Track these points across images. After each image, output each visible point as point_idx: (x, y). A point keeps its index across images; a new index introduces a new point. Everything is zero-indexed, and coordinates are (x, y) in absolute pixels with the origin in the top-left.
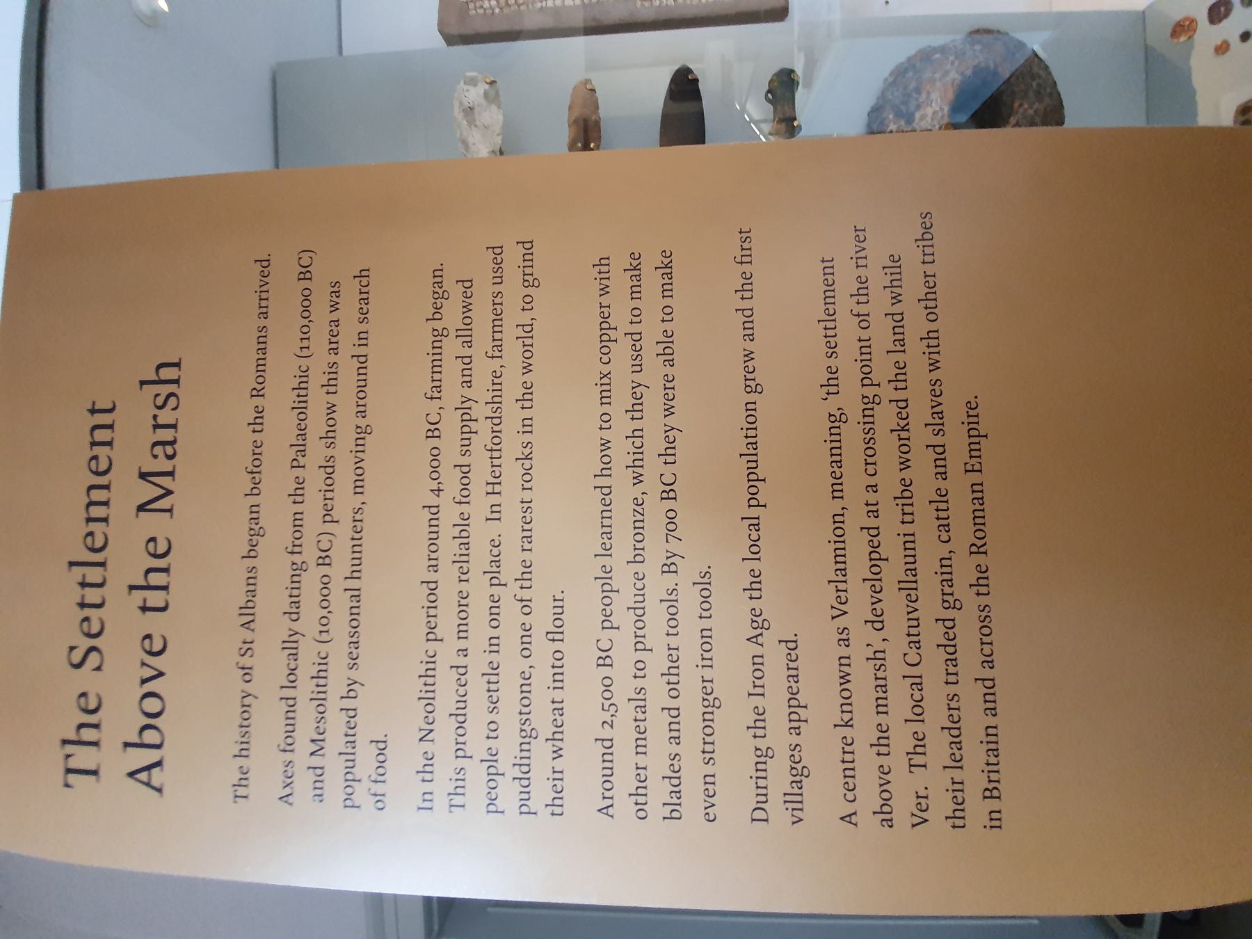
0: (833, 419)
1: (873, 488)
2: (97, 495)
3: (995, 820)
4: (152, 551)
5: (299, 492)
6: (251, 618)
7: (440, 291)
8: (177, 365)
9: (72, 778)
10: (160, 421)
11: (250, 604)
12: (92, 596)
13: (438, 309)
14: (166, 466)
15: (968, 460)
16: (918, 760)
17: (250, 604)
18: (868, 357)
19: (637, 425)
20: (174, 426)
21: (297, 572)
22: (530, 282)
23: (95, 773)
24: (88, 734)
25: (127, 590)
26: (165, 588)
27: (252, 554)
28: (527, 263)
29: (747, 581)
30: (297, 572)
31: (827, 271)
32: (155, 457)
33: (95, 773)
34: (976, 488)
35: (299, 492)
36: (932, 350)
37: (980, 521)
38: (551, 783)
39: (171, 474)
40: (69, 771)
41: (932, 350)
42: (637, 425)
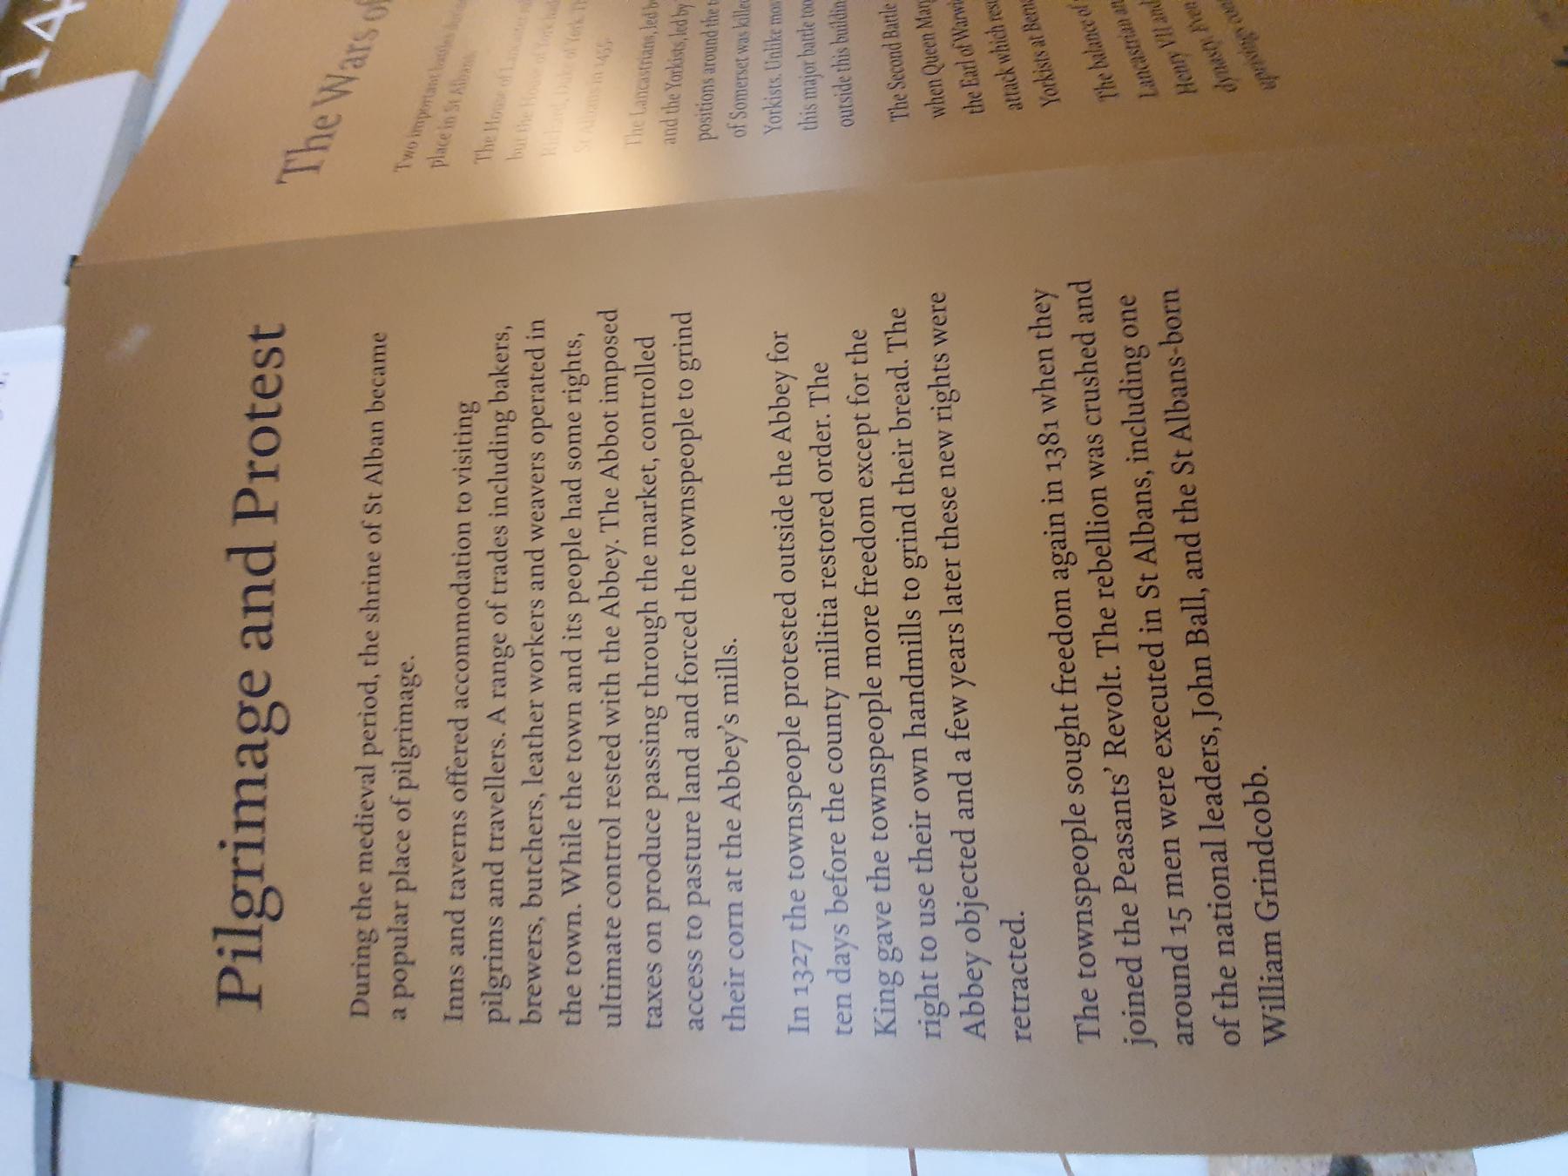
4: (247, 688)
6: (377, 469)
11: (377, 454)
15: (1259, 897)
17: (377, 454)
19: (612, 668)
21: (501, 660)
22: (689, 362)
27: (378, 406)
30: (501, 660)
36: (611, 698)
37: (1065, 605)
41: (611, 698)
42: (612, 668)
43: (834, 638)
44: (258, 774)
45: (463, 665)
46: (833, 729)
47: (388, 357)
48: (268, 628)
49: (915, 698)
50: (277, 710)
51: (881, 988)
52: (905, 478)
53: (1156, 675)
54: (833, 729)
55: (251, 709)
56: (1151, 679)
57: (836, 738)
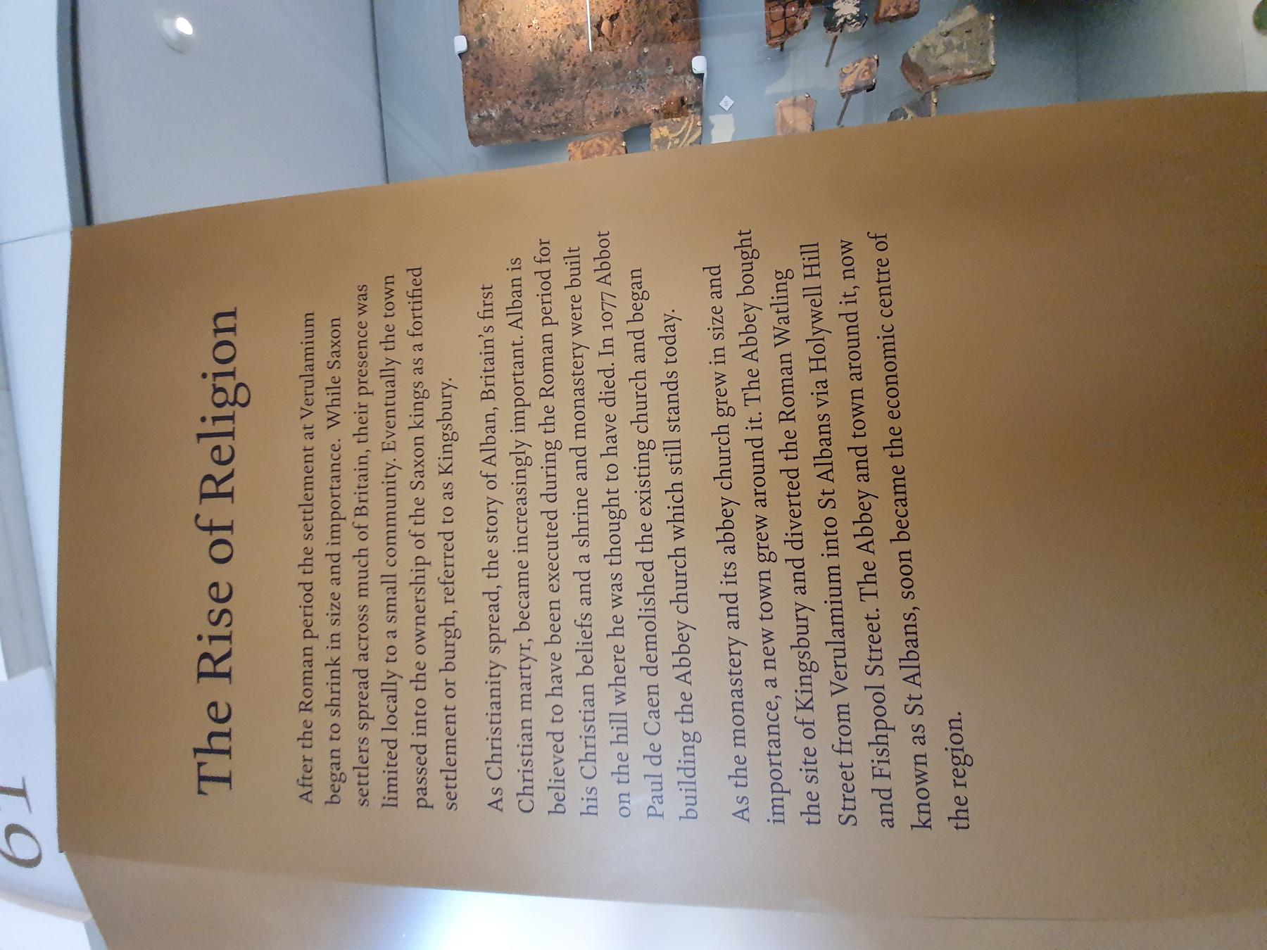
2: (309, 480)
3: (960, 818)
4: (217, 458)
5: (419, 513)
7: (640, 292)
8: (233, 314)
9: (205, 786)
12: (308, 516)
13: (638, 311)
16: (868, 588)
18: (892, 353)
23: (227, 780)
24: (218, 743)
31: (883, 291)
33: (227, 780)
34: (784, 358)
35: (419, 513)
38: (357, 416)
40: (202, 778)
43: (784, 300)
45: (391, 552)
47: (316, 323)
50: (242, 389)
55: (222, 390)
57: (760, 469)
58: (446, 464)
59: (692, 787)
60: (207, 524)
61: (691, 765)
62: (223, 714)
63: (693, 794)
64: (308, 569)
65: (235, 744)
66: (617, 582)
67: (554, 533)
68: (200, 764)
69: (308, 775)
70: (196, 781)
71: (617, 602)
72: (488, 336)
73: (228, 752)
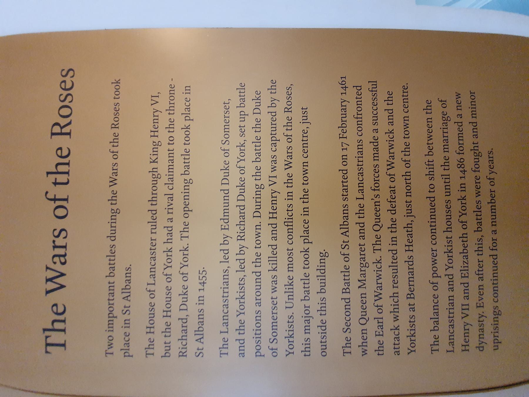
0: (322, 255)
1: (376, 131)
4: (60, 154)
7: (364, 263)
10: (57, 244)
14: (364, 279)
20: (65, 247)
25: (42, 331)
26: (68, 173)
28: (113, 221)
29: (425, 105)
32: (55, 263)
33: (64, 345)
39: (365, 280)
40: (47, 345)
43: (292, 290)
44: (172, 164)
46: (258, 284)
48: (64, 256)
49: (274, 232)
51: (170, 351)
52: (305, 197)
53: (358, 97)
54: (258, 284)
56: (357, 98)
58: (154, 158)
59: (324, 278)
60: (53, 197)
61: (323, 268)
62: (187, 224)
63: (324, 281)
64: (154, 203)
65: (68, 325)
66: (275, 279)
67: (360, 97)
68: (47, 337)
69: (481, 269)
70: (44, 346)
71: (274, 290)
72: (377, 200)
73: (64, 330)
